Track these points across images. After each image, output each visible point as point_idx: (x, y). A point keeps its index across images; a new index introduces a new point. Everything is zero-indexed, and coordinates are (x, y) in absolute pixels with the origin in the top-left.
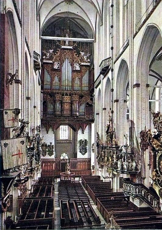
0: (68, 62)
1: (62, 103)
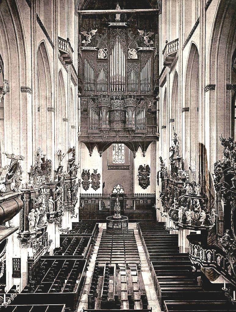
0: (90, 66)
1: (110, 111)
